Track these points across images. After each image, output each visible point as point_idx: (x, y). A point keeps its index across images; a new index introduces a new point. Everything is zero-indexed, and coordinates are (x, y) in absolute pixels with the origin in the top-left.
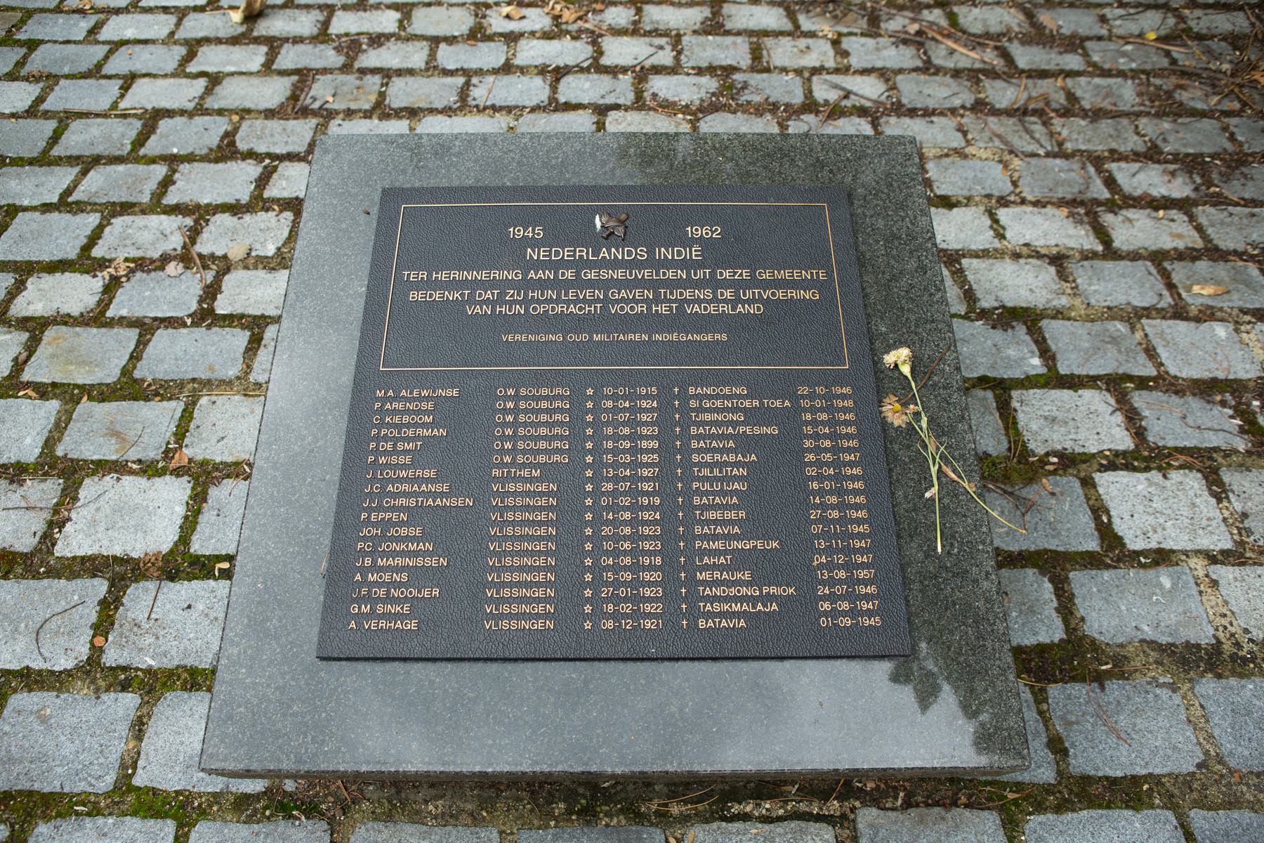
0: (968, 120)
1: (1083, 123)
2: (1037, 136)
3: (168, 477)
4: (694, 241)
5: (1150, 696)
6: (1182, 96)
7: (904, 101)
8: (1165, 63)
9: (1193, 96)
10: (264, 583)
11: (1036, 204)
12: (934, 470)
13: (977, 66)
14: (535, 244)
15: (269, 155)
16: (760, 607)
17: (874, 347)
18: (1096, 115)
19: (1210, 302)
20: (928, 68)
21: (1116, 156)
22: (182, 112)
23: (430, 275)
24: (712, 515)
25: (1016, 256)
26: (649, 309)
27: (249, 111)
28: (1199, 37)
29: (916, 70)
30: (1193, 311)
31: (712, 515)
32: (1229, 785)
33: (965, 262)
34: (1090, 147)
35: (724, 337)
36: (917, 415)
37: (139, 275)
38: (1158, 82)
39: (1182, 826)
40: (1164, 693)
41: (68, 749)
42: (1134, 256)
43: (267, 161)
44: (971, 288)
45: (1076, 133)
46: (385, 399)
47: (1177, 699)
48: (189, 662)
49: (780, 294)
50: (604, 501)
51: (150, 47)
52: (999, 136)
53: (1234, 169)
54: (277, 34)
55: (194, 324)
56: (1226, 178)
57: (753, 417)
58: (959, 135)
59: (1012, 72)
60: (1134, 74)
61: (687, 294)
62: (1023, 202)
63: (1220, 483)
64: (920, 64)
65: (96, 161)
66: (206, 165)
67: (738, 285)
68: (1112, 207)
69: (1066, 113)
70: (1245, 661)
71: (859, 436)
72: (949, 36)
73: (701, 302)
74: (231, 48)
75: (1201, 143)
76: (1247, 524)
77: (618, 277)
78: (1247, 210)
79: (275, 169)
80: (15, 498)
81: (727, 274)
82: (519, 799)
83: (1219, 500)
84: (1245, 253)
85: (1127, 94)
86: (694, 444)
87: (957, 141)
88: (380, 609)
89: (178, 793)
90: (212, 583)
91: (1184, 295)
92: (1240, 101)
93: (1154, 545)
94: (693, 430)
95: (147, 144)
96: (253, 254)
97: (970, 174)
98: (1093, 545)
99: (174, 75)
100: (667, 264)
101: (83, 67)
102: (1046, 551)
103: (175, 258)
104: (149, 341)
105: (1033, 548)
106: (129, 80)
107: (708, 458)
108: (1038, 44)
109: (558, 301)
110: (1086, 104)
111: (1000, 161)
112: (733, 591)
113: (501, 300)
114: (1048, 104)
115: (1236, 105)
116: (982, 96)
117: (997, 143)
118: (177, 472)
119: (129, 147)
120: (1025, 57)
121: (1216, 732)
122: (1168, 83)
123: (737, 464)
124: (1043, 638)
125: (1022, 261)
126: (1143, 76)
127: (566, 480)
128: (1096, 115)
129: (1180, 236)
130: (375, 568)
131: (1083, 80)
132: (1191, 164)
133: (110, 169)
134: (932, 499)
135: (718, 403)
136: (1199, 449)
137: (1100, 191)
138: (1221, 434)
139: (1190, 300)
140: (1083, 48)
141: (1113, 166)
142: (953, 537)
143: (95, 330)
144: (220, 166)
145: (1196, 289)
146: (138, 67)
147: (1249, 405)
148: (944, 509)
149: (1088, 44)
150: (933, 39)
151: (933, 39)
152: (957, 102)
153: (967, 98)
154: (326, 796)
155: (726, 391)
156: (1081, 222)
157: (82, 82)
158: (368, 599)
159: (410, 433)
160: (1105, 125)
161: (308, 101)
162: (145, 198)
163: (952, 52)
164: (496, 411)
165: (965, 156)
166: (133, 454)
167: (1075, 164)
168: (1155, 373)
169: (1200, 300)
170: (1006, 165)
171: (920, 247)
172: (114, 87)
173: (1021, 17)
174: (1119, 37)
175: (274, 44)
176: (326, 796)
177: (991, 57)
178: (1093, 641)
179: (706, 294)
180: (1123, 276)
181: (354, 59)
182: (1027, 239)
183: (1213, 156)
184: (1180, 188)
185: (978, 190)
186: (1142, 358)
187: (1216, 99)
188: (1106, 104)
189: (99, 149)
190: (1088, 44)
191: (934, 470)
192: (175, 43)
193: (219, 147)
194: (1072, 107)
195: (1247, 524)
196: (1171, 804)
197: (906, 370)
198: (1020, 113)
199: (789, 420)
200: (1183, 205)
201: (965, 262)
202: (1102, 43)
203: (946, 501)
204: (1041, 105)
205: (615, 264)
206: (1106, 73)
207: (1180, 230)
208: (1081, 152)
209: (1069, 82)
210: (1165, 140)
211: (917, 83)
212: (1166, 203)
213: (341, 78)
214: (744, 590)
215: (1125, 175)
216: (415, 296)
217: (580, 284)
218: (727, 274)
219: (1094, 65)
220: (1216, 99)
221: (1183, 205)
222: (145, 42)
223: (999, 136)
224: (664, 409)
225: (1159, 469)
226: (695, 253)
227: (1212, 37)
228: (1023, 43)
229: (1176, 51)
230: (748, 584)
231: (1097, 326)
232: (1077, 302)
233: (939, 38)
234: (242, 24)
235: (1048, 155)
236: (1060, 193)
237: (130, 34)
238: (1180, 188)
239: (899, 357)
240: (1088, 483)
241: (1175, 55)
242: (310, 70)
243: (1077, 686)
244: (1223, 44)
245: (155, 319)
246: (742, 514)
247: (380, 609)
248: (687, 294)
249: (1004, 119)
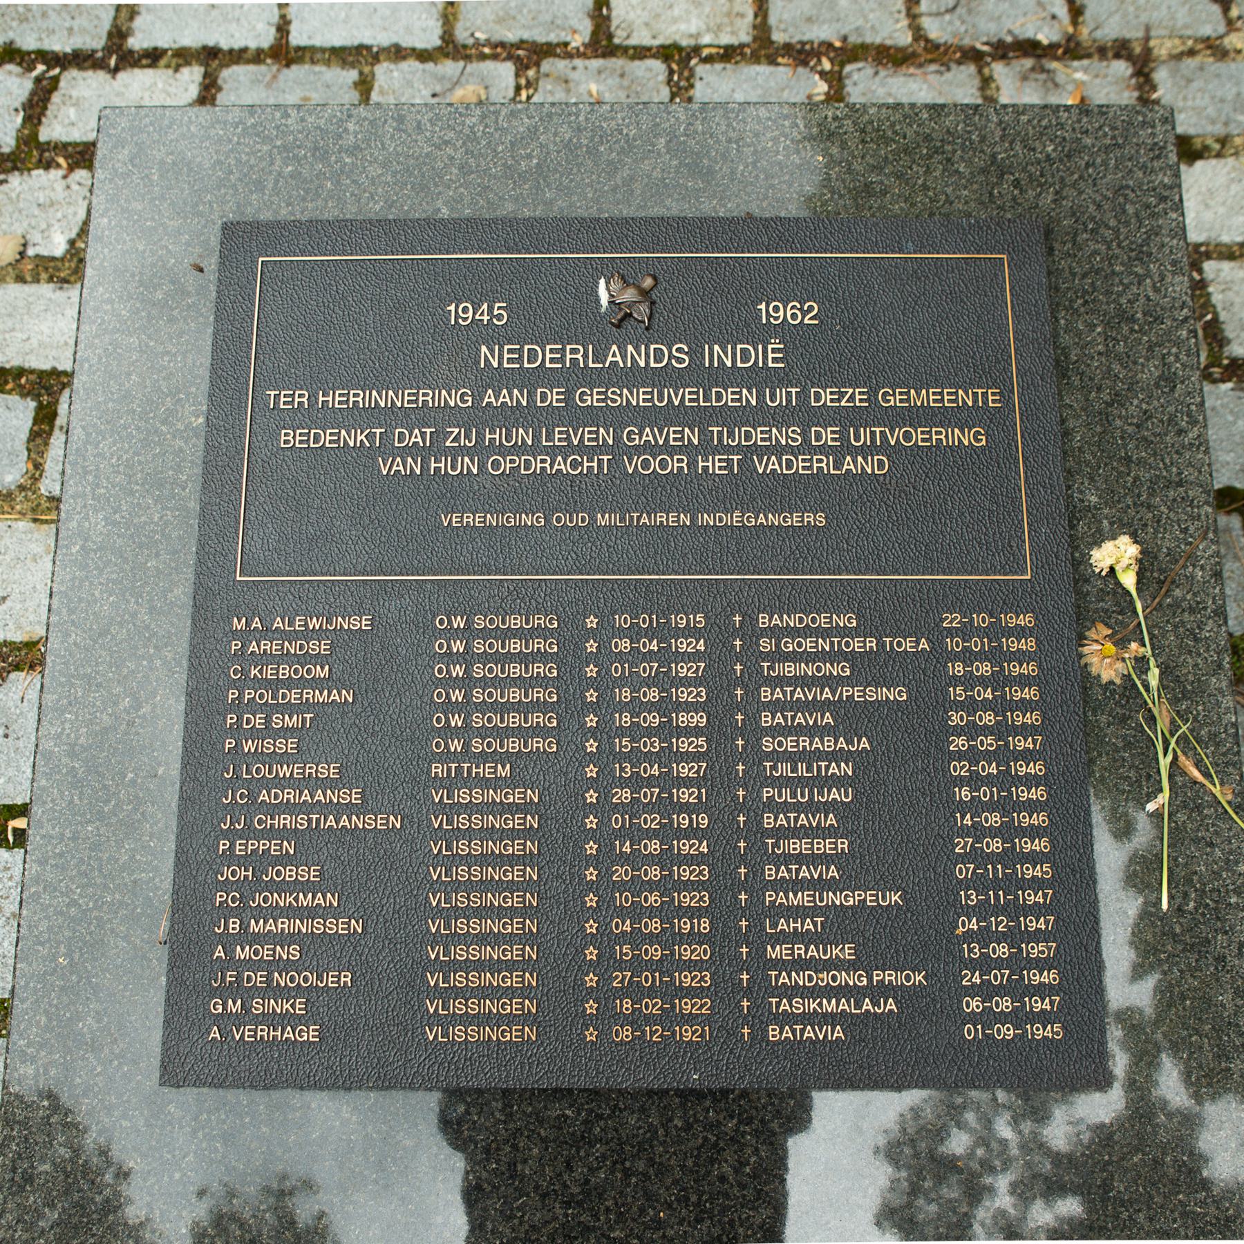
12: (1164, 763)
16: (867, 1005)
36: (1141, 664)
73: (786, 453)
88: (257, 1007)
94: (765, 694)
113: (435, 448)
142: (1189, 881)
158: (235, 990)
199: (927, 677)
205: (632, 377)
226: (771, 355)
230: (850, 966)
246: (843, 844)
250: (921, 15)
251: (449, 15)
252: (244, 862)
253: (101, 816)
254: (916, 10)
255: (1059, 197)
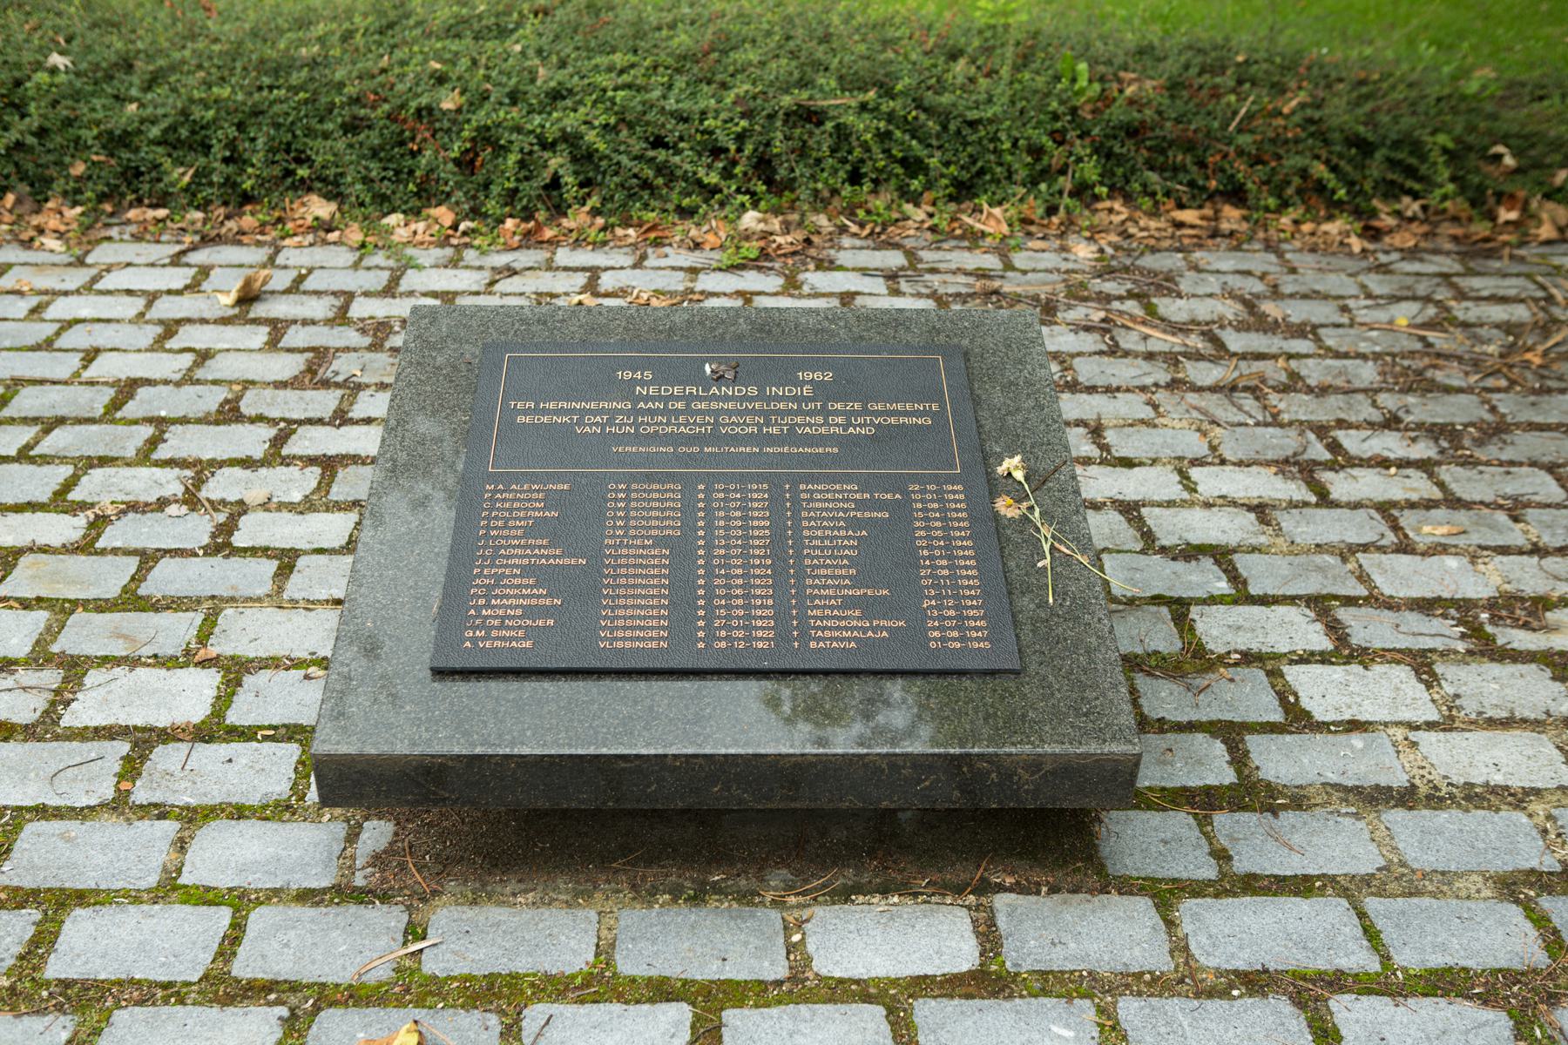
0: (1161, 396)
1: (1306, 398)
2: (1246, 408)
3: (192, 669)
4: (804, 382)
5: (1331, 823)
6: (1439, 376)
7: (1081, 379)
8: (1418, 346)
9: (1451, 375)
10: (374, 622)
11: (1240, 464)
12: (1046, 548)
13: (1177, 349)
14: (643, 383)
15: (283, 419)
16: (870, 634)
17: (987, 460)
18: (1323, 391)
19: (1443, 540)
20: (1114, 351)
21: (1342, 424)
22: (166, 382)
23: (537, 404)
24: (823, 572)
25: (1208, 505)
26: (760, 430)
27: (253, 383)
28: (1465, 325)
29: (1101, 353)
30: (1421, 547)
31: (823, 572)
32: (1411, 881)
33: (1144, 511)
34: (1313, 418)
35: (836, 450)
36: (1031, 508)
37: (131, 515)
38: (1406, 363)
39: (1355, 908)
40: (1347, 821)
41: (100, 859)
42: (1356, 506)
43: (282, 425)
44: (1150, 530)
45: (1297, 407)
46: (495, 491)
47: (1361, 824)
48: (234, 800)
49: (892, 420)
50: (716, 562)
51: (114, 326)
52: (1195, 408)
53: (1491, 436)
54: (281, 316)
55: (205, 554)
56: (1479, 443)
57: (861, 505)
58: (1149, 408)
59: (1220, 351)
60: (1377, 356)
61: (799, 420)
62: (1223, 462)
63: (1433, 674)
64: (1105, 348)
65: (61, 421)
66: (205, 427)
67: (848, 414)
68: (1332, 466)
69: (1284, 389)
70: (1442, 799)
71: (971, 518)
72: (1144, 323)
73: (812, 425)
74: (222, 328)
75: (1454, 415)
76: (1458, 702)
77: (732, 407)
78: (1502, 469)
79: (294, 431)
80: (9, 682)
81: (839, 406)
82: (618, 891)
83: (1429, 686)
84: (1495, 502)
85: (1367, 373)
86: (805, 523)
87: (1148, 412)
88: (494, 633)
89: (231, 890)
90: (254, 744)
91: (1411, 535)
92: (1508, 379)
93: (1347, 717)
94: (804, 514)
95: (125, 408)
96: (275, 500)
97: (1159, 440)
98: (1277, 716)
99: (151, 349)
100: (777, 398)
101: (31, 342)
102: (1220, 721)
103: (176, 501)
104: (152, 568)
105: (1204, 719)
106: (91, 355)
107: (819, 533)
108: (1257, 330)
109: (668, 424)
110: (1312, 382)
111: (1199, 430)
112: (843, 624)
113: (611, 422)
114: (1263, 381)
115: (1503, 383)
116: (1180, 375)
117: (1195, 414)
118: (203, 664)
119: (102, 411)
120: (1235, 342)
121: (1401, 846)
122: (1418, 364)
123: (848, 538)
124: (1212, 780)
125: (1215, 509)
126: (1388, 359)
127: (680, 550)
128: (1323, 391)
129: (1414, 490)
130: (488, 606)
131: (1310, 362)
132: (1435, 431)
133: (77, 428)
134: (1045, 568)
135: (829, 496)
136: (1410, 650)
137: (1319, 451)
138: (1439, 639)
139: (1417, 539)
140: (1315, 334)
141: (1340, 435)
142: (1066, 593)
143: (83, 558)
144: (222, 428)
145: (1426, 529)
146: (100, 342)
147: (1476, 617)
148: (1056, 577)
149: (1322, 331)
150: (1123, 326)
151: (1123, 326)
152: (1148, 381)
153: (1163, 377)
154: (401, 889)
155: (838, 487)
156: (1293, 478)
157: (30, 354)
158: (482, 627)
159: (522, 514)
160: (1334, 400)
161: (329, 374)
162: (130, 453)
163: (1146, 338)
164: (606, 500)
165: (1155, 426)
166: (146, 651)
167: (1293, 433)
168: (1366, 593)
169: (1431, 539)
170: (1204, 434)
171: (1038, 391)
172: (75, 361)
173: (1239, 307)
174: (1362, 324)
175: (277, 328)
176: (401, 889)
177: (1195, 342)
178: (1269, 784)
179: (820, 420)
180: (1339, 520)
181: (383, 340)
182: (1224, 492)
183: (1466, 426)
184: (1423, 450)
185: (1166, 453)
186: (1353, 581)
187: (1477, 377)
188: (1340, 382)
189: (61, 412)
190: (1322, 331)
191: (1046, 548)
192: (147, 322)
193: (218, 411)
194: (1294, 383)
195: (1458, 702)
196: (1344, 892)
197: (1019, 475)
198: (1229, 389)
199: (902, 511)
200: (1425, 466)
201: (1144, 511)
202: (1340, 331)
203: (1059, 569)
204: (1256, 382)
205: (726, 398)
206: (1338, 355)
207: (1415, 485)
208: (1301, 423)
209: (1293, 364)
210: (1408, 412)
211: (1099, 365)
212: (1404, 464)
213: (369, 356)
214: (854, 623)
215: (1351, 441)
216: (520, 419)
217: (688, 411)
218: (839, 406)
219: (1329, 349)
220: (1477, 377)
221: (1425, 466)
222: (108, 321)
223: (1195, 408)
224: (775, 503)
225: (1361, 663)
226: (807, 391)
227: (1481, 325)
228: (1238, 330)
229: (1431, 336)
230: (859, 618)
231: (1302, 559)
232: (1280, 541)
233: (1130, 324)
234: (233, 306)
235: (1257, 424)
236: (1270, 456)
237: (84, 313)
238: (1423, 450)
239: (1013, 465)
240: (1274, 674)
241: (1431, 340)
242: (327, 349)
243: (1247, 815)
244: (1495, 331)
245: (158, 550)
246: (853, 571)
247: (494, 633)
248: (799, 420)
249: (1207, 395)
250: (1214, 203)
251: (511, 1031)
252: (490, 576)
253: (398, 567)
254: (1217, 198)
255: (972, 341)
